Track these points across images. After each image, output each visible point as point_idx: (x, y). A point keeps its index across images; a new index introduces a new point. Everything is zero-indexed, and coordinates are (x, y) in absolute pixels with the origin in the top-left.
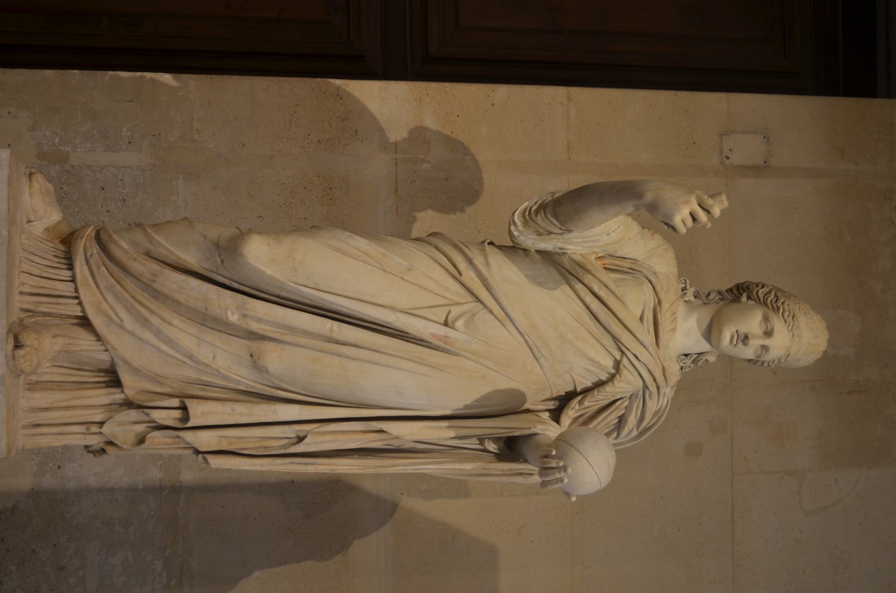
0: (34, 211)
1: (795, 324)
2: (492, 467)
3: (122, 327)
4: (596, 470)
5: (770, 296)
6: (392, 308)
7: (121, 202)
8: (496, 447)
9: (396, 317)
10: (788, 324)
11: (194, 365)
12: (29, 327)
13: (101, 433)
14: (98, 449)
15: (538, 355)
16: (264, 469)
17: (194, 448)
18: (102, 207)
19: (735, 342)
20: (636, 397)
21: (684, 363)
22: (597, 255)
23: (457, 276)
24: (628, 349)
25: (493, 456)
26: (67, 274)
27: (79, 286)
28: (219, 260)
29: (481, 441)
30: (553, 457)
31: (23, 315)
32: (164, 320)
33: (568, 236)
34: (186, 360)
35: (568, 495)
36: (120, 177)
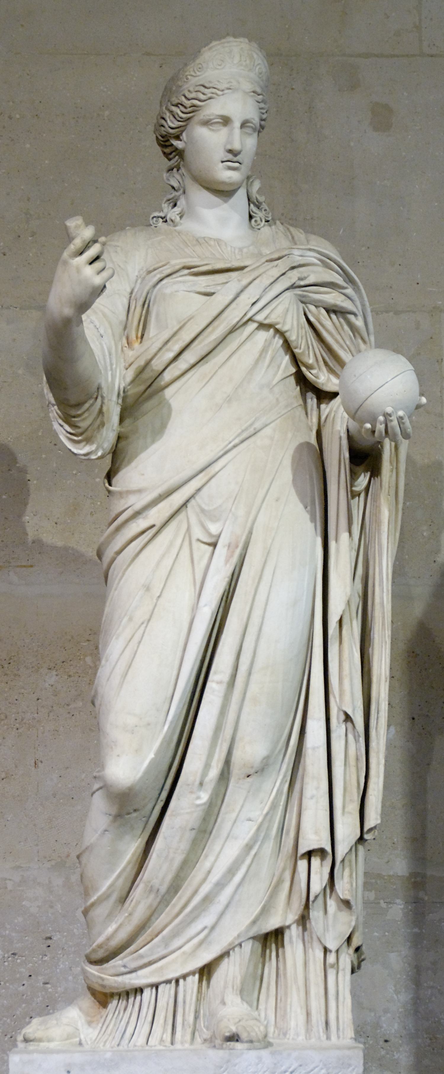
0: (69, 1037)
2: (387, 484)
3: (213, 928)
4: (389, 379)
6: (195, 608)
7: (17, 959)
8: (363, 475)
9: (205, 605)
10: (214, 95)
11: (259, 843)
12: (214, 1032)
13: (337, 951)
14: (356, 955)
15: (251, 430)
16: (383, 761)
17: (356, 843)
18: (24, 985)
19: (236, 165)
20: (304, 296)
21: (261, 221)
22: (126, 347)
24: (245, 314)
25: (374, 479)
26: (148, 994)
28: (135, 815)
29: (355, 495)
30: (374, 426)
31: (198, 1040)
32: (204, 880)
33: (105, 391)
34: (253, 852)
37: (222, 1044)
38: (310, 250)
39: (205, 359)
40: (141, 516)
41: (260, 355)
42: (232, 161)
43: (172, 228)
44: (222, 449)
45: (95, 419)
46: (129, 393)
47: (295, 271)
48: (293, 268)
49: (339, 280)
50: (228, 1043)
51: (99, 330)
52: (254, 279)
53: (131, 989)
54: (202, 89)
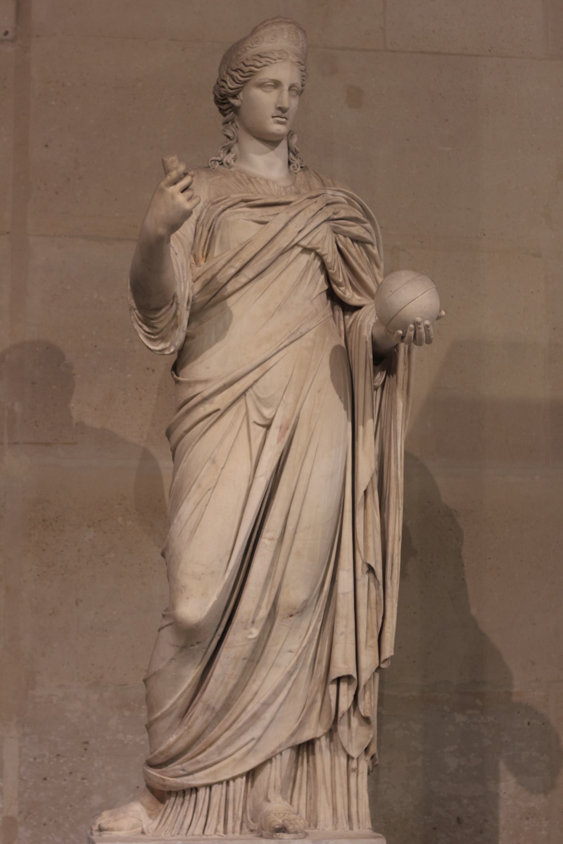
0: (134, 827)
1: (269, 56)
3: (259, 739)
4: (420, 294)
5: (237, 78)
9: (261, 476)
10: (268, 63)
11: (298, 670)
13: (358, 759)
15: (298, 334)
19: (284, 120)
22: (193, 264)
23: (219, 414)
24: (293, 240)
25: (389, 376)
26: (202, 793)
27: (217, 780)
28: (197, 646)
33: (179, 298)
35: (439, 318)
36: (31, 760)
37: (272, 835)
38: (339, 191)
39: (261, 275)
40: (207, 402)
41: (304, 273)
42: (281, 117)
43: (227, 170)
44: (276, 349)
45: (171, 321)
46: (197, 301)
47: (330, 207)
48: (328, 205)
49: (360, 216)
50: (278, 834)
51: (174, 249)
52: (300, 212)
53: (188, 789)
54: (257, 58)
